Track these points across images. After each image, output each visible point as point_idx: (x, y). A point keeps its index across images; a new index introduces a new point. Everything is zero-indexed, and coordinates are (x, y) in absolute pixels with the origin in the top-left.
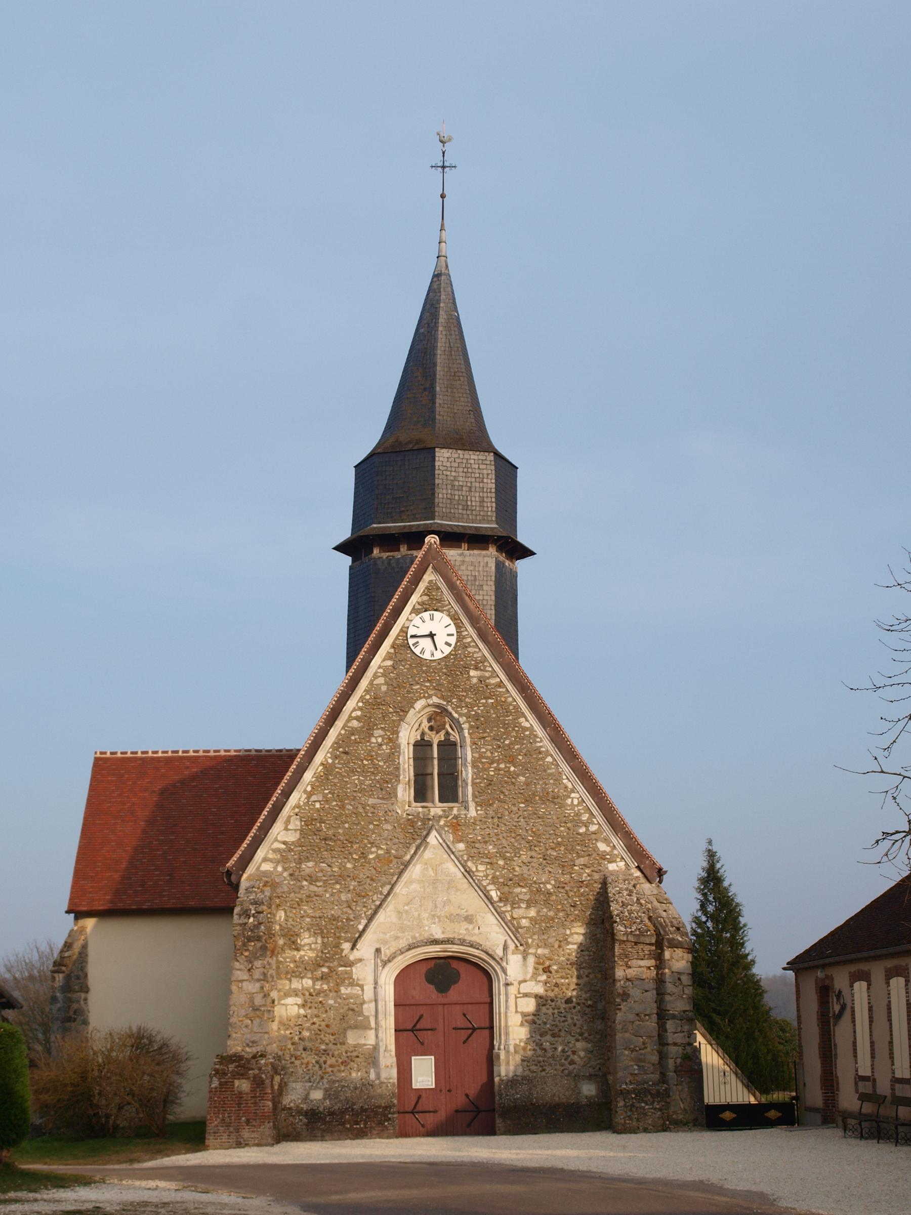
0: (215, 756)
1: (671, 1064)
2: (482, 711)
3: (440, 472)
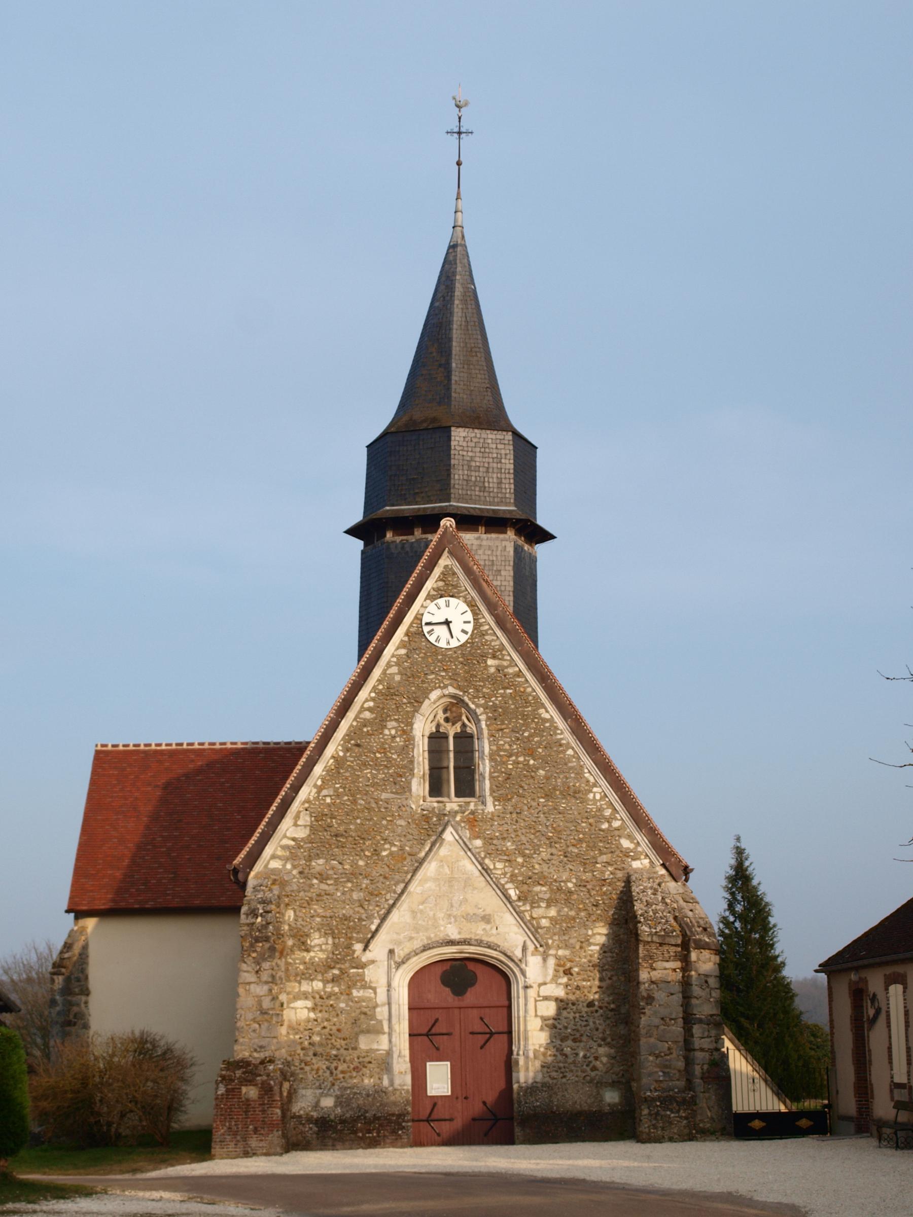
0: (221, 749)
1: (697, 1070)
2: (500, 701)
3: (457, 453)
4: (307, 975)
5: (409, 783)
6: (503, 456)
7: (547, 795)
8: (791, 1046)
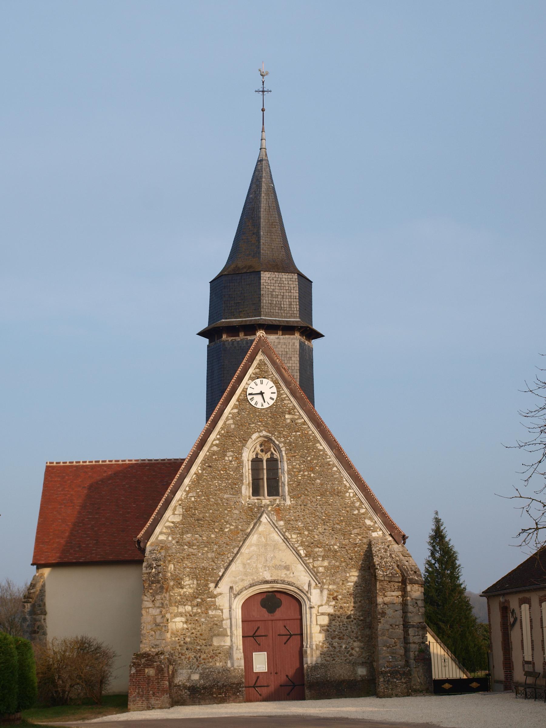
0: (123, 464)
1: (412, 655)
2: (293, 439)
3: (264, 287)
4: (182, 603)
5: (240, 489)
6: (292, 288)
7: (321, 495)
8: (470, 638)
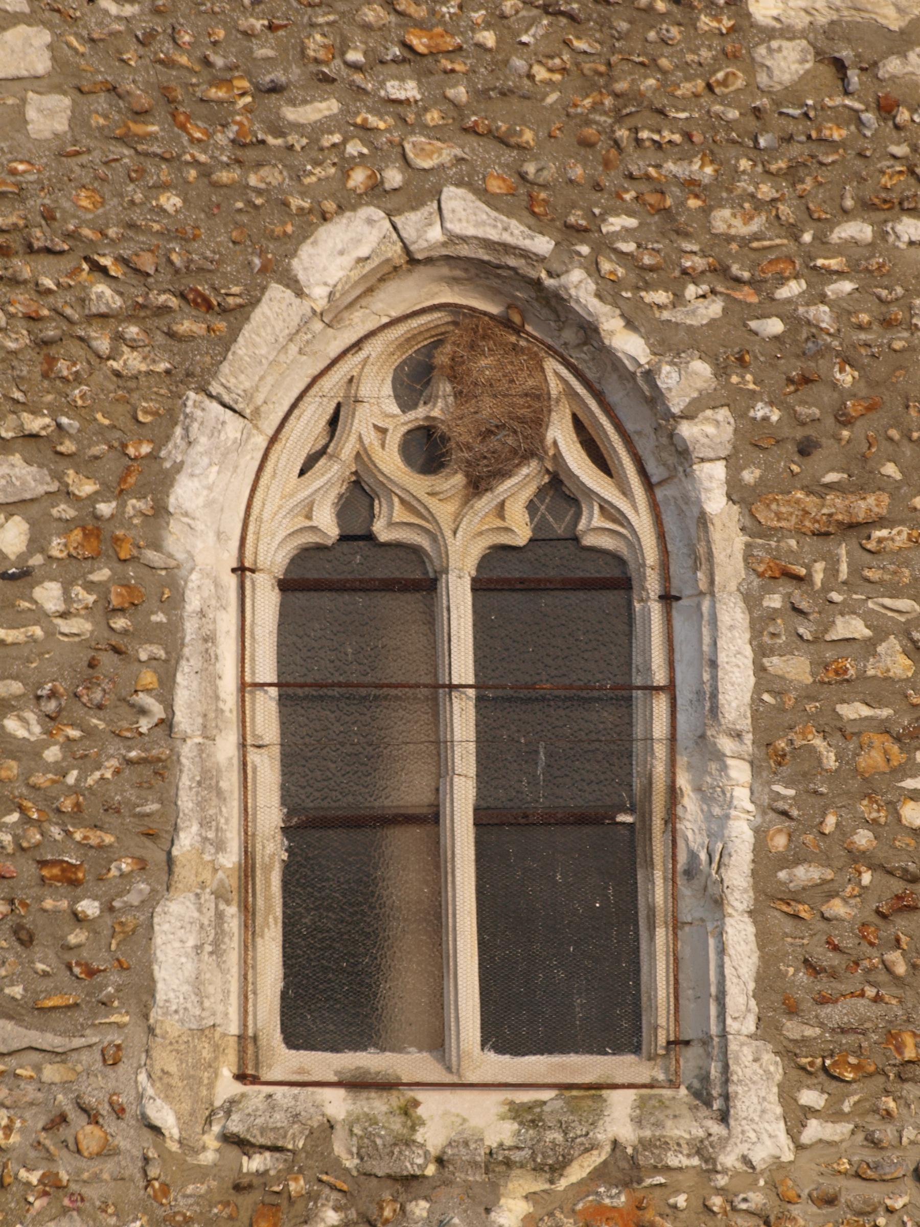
2: (842, 310)
